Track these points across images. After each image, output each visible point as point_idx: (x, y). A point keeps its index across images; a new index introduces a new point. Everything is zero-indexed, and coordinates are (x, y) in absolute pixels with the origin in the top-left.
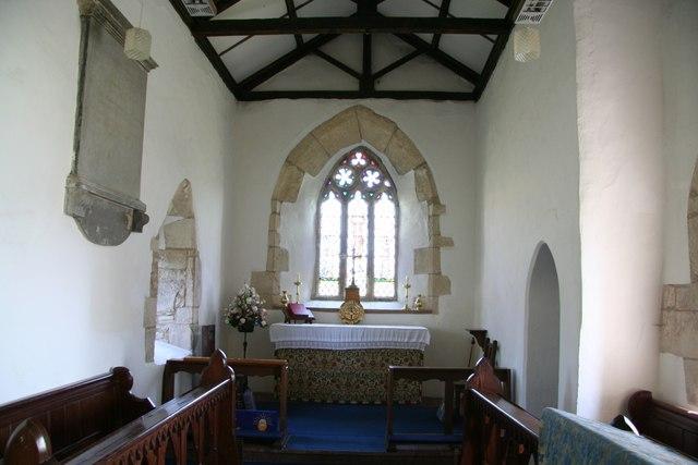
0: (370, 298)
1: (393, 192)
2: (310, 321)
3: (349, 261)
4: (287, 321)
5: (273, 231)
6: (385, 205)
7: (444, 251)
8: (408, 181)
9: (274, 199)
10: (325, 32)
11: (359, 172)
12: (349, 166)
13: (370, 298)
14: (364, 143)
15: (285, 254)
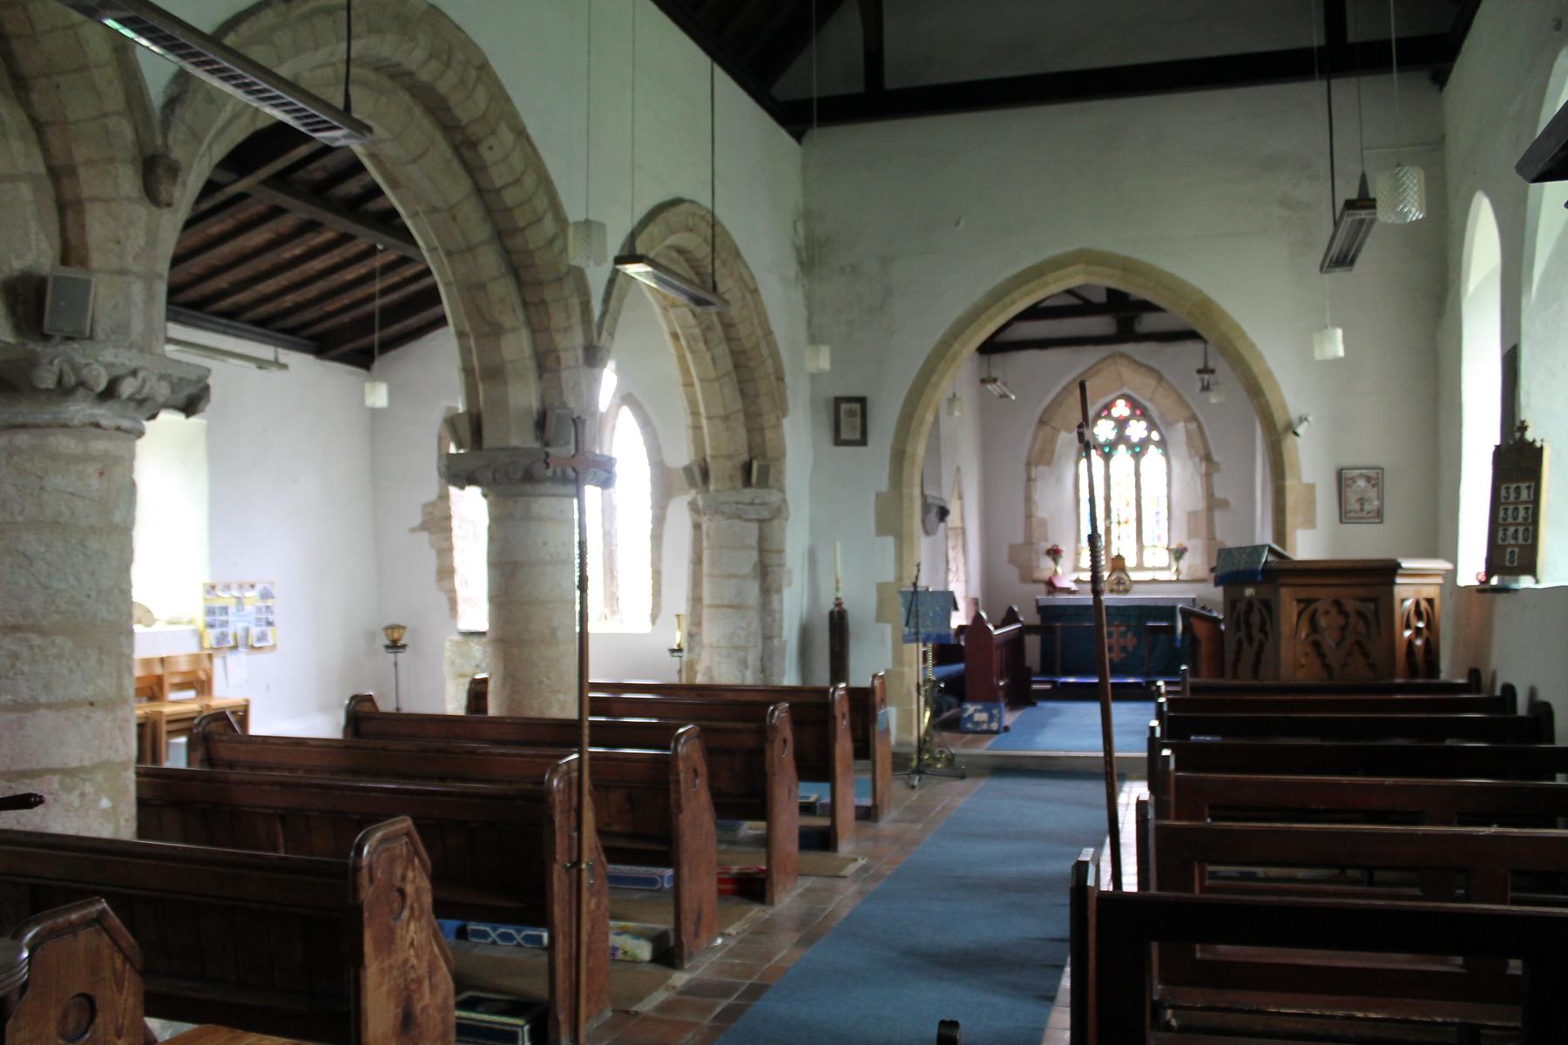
0: (1140, 567)
1: (1162, 444)
2: (1074, 592)
3: (1114, 527)
4: (1049, 593)
5: (1028, 499)
6: (1154, 459)
7: (1217, 514)
8: (1179, 433)
9: (1029, 464)
10: (220, 197)
11: (1122, 424)
12: (1109, 416)
13: (1140, 567)
14: (1126, 390)
15: (1043, 523)
